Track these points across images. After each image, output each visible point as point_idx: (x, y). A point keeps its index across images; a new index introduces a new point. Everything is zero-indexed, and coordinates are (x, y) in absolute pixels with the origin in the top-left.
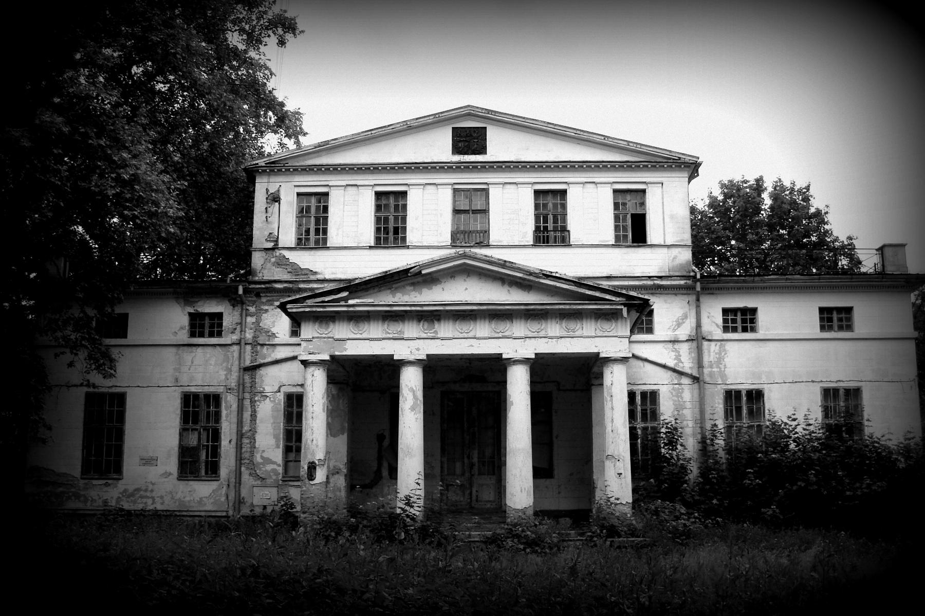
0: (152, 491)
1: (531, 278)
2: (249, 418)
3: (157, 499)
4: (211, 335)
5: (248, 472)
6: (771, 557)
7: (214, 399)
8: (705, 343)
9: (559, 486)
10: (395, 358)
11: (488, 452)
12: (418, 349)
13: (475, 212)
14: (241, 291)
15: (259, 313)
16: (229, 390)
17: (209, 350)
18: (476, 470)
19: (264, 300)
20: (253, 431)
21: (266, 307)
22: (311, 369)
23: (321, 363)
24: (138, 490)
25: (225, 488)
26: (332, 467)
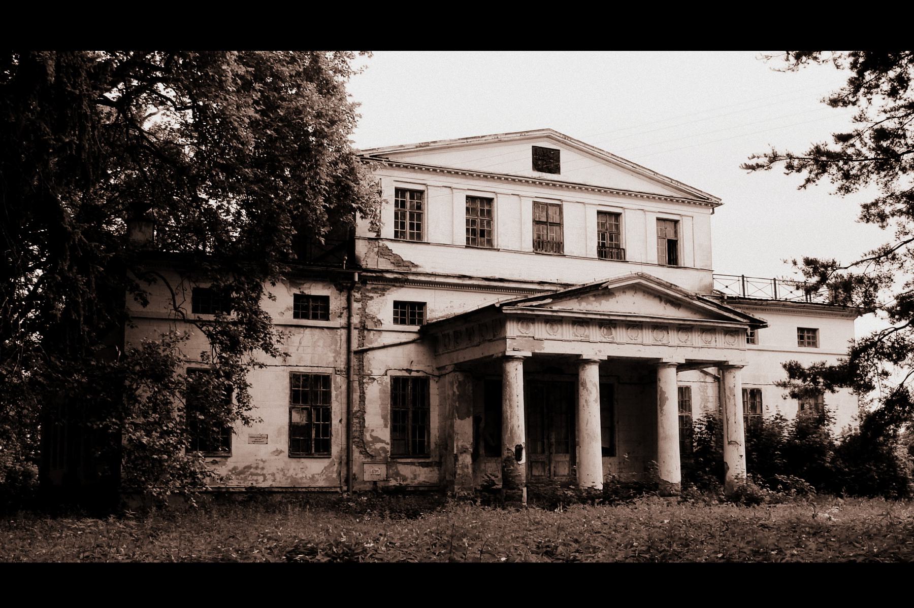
0: (263, 469)
1: (687, 299)
3: (268, 477)
4: (315, 317)
6: (823, 515)
7: (325, 380)
13: (552, 224)
15: (364, 299)
18: (553, 449)
19: (369, 287)
20: (363, 411)
21: (371, 295)
24: (249, 467)
25: (336, 465)
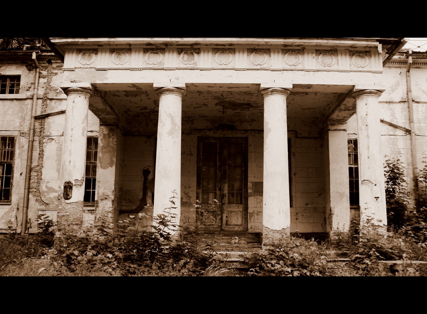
2: (37, 156)
4: (11, 92)
5: (35, 199)
8: (415, 105)
9: (297, 214)
10: (155, 86)
11: (237, 185)
12: (177, 79)
14: (34, 56)
16: (22, 134)
17: (8, 102)
18: (226, 200)
19: (54, 65)
20: (40, 166)
22: (73, 97)
23: (83, 90)
26: (101, 194)
